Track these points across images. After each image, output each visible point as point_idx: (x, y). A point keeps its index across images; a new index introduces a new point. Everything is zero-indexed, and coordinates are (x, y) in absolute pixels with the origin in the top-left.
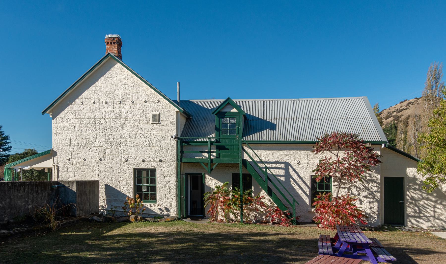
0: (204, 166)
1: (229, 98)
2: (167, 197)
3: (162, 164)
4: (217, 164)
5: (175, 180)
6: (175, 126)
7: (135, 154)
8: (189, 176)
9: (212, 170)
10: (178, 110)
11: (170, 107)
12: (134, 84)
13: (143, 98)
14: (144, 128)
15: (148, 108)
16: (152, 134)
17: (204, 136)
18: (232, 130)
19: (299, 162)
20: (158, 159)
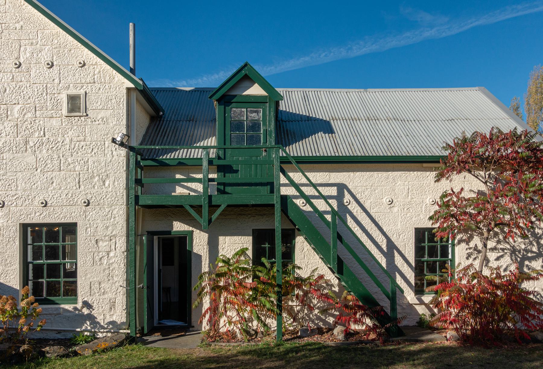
0: (192, 212)
1: (246, 65)
2: (104, 286)
3: (92, 213)
4: (223, 207)
5: (124, 248)
6: (124, 122)
7: (25, 191)
8: (155, 238)
9: (210, 221)
10: (132, 86)
11: (112, 78)
12: (21, 23)
13: (45, 57)
14: (48, 125)
15: (57, 81)
16: (68, 140)
17: (190, 144)
18: (252, 136)
19: (392, 202)
20: (81, 199)
